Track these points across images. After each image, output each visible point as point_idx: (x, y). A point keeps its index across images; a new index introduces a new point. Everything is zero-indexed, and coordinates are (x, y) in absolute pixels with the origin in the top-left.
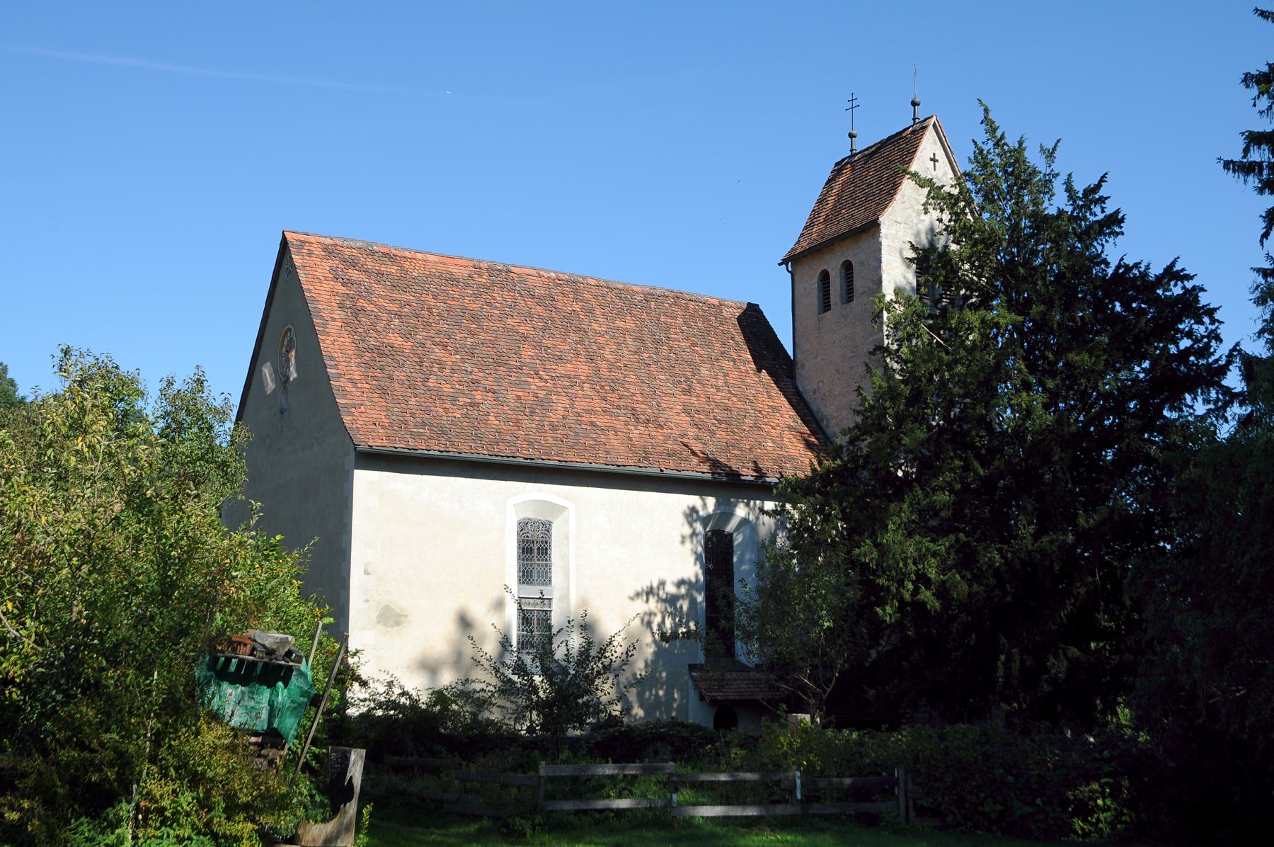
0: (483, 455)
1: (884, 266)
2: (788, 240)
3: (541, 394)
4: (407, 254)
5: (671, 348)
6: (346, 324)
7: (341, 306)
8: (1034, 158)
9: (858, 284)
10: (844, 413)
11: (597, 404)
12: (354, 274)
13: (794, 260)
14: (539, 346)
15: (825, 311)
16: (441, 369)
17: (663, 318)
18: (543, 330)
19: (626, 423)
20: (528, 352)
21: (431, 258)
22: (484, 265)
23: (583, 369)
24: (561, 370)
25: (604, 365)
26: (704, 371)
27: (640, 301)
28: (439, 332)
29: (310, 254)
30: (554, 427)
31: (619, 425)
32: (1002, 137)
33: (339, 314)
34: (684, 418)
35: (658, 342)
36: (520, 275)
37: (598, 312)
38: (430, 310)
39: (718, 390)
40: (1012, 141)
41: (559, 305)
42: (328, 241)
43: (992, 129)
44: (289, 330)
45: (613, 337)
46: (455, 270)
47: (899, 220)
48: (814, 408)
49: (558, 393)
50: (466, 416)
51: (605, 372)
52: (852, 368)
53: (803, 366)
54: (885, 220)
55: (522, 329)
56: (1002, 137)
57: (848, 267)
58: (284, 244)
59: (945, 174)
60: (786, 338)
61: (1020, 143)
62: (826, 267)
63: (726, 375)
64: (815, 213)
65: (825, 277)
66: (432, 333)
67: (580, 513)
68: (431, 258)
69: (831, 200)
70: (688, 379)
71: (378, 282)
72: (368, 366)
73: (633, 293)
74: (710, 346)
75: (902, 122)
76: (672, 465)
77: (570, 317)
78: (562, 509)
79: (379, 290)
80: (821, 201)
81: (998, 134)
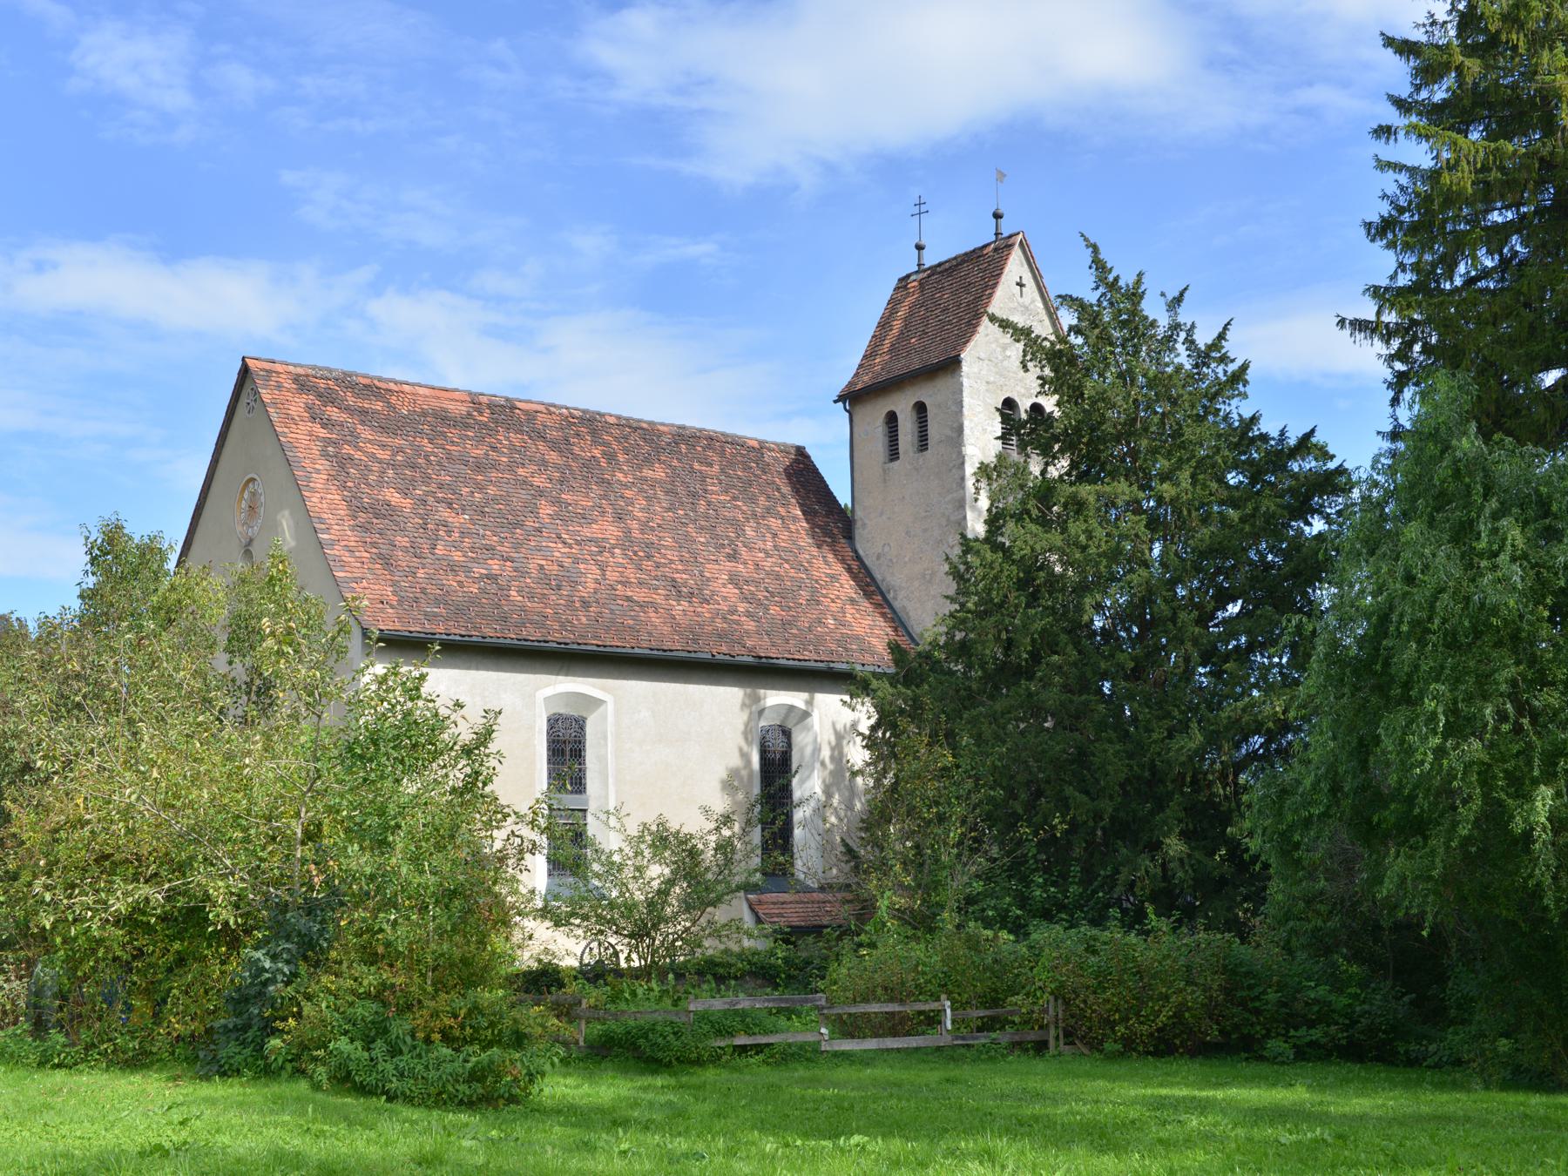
0: (511, 636)
1: (965, 411)
2: (844, 369)
3: (567, 562)
4: (392, 386)
5: (709, 504)
6: (332, 478)
7: (325, 454)
8: (1154, 309)
10: (916, 584)
11: (632, 574)
12: (334, 413)
13: (853, 398)
14: (557, 502)
15: (892, 460)
16: (449, 532)
17: (696, 466)
18: (561, 483)
19: (667, 598)
20: (546, 510)
21: (421, 391)
22: (484, 400)
23: (611, 531)
24: (587, 532)
25: (635, 525)
26: (749, 532)
27: (669, 444)
28: (441, 486)
29: (279, 387)
30: (585, 604)
31: (659, 600)
32: (1116, 279)
33: (322, 465)
34: (731, 590)
35: (694, 495)
36: (526, 412)
37: (621, 458)
38: (427, 457)
39: (768, 555)
40: (1127, 280)
41: (576, 450)
42: (300, 371)
43: (1099, 266)
44: (253, 480)
45: (641, 491)
46: (451, 406)
47: (983, 356)
48: (878, 577)
49: (585, 561)
50: (483, 591)
51: (636, 534)
52: (925, 530)
53: (864, 525)
54: (967, 356)
55: (537, 481)
56: (1116, 279)
57: (921, 408)
58: (245, 372)
59: (1033, 301)
60: (843, 497)
61: (1139, 282)
62: (893, 408)
63: (775, 535)
64: (877, 340)
65: (892, 418)
66: (433, 488)
67: (621, 708)
68: (421, 391)
69: (897, 325)
70: (732, 542)
71: (363, 423)
72: (364, 528)
73: (660, 434)
74: (753, 500)
75: (980, 235)
76: (724, 649)
77: (589, 464)
78: (598, 703)
79: (366, 433)
80: (884, 324)
81: (1111, 278)
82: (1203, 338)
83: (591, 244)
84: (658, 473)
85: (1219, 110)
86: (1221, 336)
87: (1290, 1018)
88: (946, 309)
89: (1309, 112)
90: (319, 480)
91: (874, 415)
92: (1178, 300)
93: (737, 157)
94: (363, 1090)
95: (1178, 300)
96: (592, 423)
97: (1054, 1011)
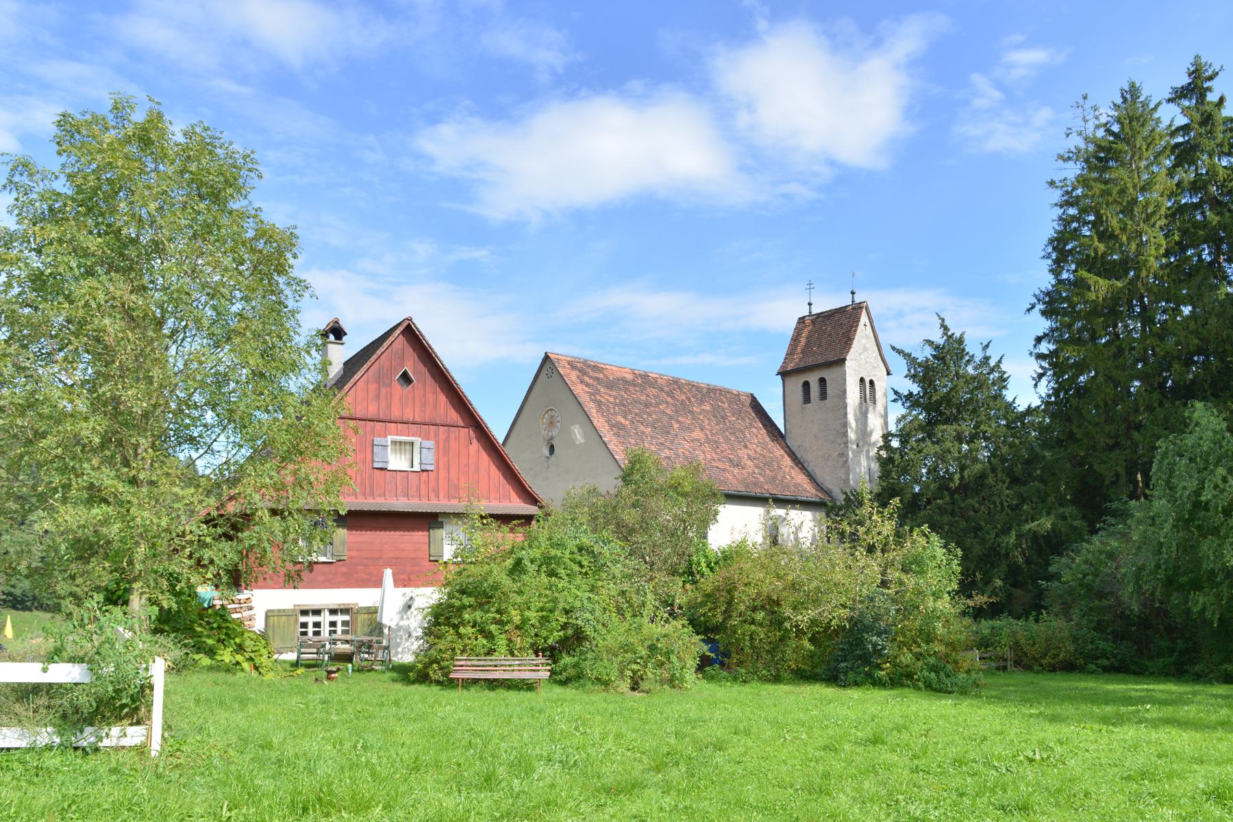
2: (777, 365)
9: (829, 391)
23: (701, 436)
57: (822, 381)
65: (806, 385)
69: (803, 341)
75: (844, 301)
82: (992, 363)
83: (423, 249)
84: (707, 407)
85: (743, 193)
86: (1000, 361)
87: (1092, 657)
88: (830, 335)
89: (785, 196)
90: (594, 411)
91: (796, 383)
92: (987, 346)
93: (496, 207)
94: (936, 690)
95: (987, 346)
96: (645, 380)
97: (1008, 654)
